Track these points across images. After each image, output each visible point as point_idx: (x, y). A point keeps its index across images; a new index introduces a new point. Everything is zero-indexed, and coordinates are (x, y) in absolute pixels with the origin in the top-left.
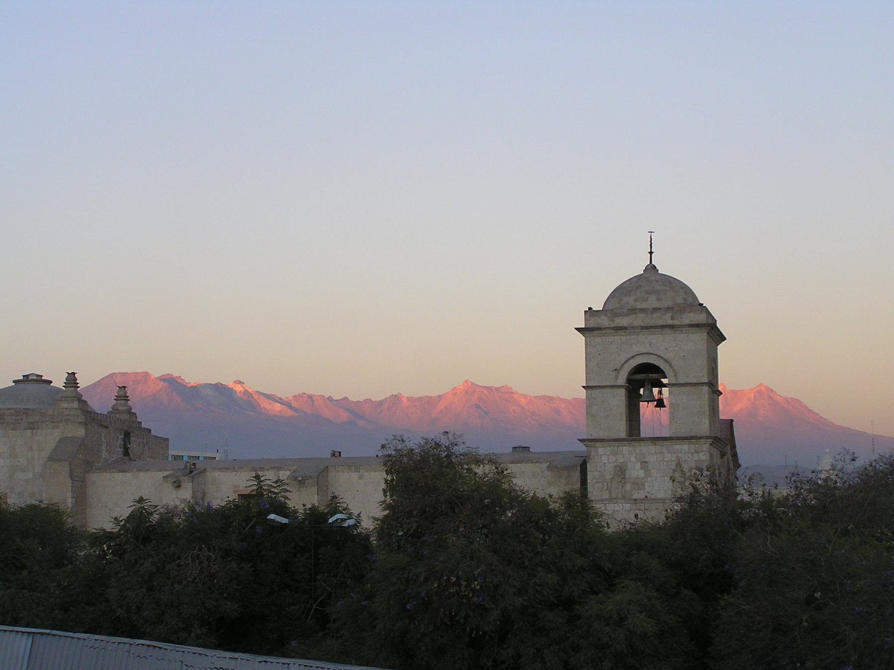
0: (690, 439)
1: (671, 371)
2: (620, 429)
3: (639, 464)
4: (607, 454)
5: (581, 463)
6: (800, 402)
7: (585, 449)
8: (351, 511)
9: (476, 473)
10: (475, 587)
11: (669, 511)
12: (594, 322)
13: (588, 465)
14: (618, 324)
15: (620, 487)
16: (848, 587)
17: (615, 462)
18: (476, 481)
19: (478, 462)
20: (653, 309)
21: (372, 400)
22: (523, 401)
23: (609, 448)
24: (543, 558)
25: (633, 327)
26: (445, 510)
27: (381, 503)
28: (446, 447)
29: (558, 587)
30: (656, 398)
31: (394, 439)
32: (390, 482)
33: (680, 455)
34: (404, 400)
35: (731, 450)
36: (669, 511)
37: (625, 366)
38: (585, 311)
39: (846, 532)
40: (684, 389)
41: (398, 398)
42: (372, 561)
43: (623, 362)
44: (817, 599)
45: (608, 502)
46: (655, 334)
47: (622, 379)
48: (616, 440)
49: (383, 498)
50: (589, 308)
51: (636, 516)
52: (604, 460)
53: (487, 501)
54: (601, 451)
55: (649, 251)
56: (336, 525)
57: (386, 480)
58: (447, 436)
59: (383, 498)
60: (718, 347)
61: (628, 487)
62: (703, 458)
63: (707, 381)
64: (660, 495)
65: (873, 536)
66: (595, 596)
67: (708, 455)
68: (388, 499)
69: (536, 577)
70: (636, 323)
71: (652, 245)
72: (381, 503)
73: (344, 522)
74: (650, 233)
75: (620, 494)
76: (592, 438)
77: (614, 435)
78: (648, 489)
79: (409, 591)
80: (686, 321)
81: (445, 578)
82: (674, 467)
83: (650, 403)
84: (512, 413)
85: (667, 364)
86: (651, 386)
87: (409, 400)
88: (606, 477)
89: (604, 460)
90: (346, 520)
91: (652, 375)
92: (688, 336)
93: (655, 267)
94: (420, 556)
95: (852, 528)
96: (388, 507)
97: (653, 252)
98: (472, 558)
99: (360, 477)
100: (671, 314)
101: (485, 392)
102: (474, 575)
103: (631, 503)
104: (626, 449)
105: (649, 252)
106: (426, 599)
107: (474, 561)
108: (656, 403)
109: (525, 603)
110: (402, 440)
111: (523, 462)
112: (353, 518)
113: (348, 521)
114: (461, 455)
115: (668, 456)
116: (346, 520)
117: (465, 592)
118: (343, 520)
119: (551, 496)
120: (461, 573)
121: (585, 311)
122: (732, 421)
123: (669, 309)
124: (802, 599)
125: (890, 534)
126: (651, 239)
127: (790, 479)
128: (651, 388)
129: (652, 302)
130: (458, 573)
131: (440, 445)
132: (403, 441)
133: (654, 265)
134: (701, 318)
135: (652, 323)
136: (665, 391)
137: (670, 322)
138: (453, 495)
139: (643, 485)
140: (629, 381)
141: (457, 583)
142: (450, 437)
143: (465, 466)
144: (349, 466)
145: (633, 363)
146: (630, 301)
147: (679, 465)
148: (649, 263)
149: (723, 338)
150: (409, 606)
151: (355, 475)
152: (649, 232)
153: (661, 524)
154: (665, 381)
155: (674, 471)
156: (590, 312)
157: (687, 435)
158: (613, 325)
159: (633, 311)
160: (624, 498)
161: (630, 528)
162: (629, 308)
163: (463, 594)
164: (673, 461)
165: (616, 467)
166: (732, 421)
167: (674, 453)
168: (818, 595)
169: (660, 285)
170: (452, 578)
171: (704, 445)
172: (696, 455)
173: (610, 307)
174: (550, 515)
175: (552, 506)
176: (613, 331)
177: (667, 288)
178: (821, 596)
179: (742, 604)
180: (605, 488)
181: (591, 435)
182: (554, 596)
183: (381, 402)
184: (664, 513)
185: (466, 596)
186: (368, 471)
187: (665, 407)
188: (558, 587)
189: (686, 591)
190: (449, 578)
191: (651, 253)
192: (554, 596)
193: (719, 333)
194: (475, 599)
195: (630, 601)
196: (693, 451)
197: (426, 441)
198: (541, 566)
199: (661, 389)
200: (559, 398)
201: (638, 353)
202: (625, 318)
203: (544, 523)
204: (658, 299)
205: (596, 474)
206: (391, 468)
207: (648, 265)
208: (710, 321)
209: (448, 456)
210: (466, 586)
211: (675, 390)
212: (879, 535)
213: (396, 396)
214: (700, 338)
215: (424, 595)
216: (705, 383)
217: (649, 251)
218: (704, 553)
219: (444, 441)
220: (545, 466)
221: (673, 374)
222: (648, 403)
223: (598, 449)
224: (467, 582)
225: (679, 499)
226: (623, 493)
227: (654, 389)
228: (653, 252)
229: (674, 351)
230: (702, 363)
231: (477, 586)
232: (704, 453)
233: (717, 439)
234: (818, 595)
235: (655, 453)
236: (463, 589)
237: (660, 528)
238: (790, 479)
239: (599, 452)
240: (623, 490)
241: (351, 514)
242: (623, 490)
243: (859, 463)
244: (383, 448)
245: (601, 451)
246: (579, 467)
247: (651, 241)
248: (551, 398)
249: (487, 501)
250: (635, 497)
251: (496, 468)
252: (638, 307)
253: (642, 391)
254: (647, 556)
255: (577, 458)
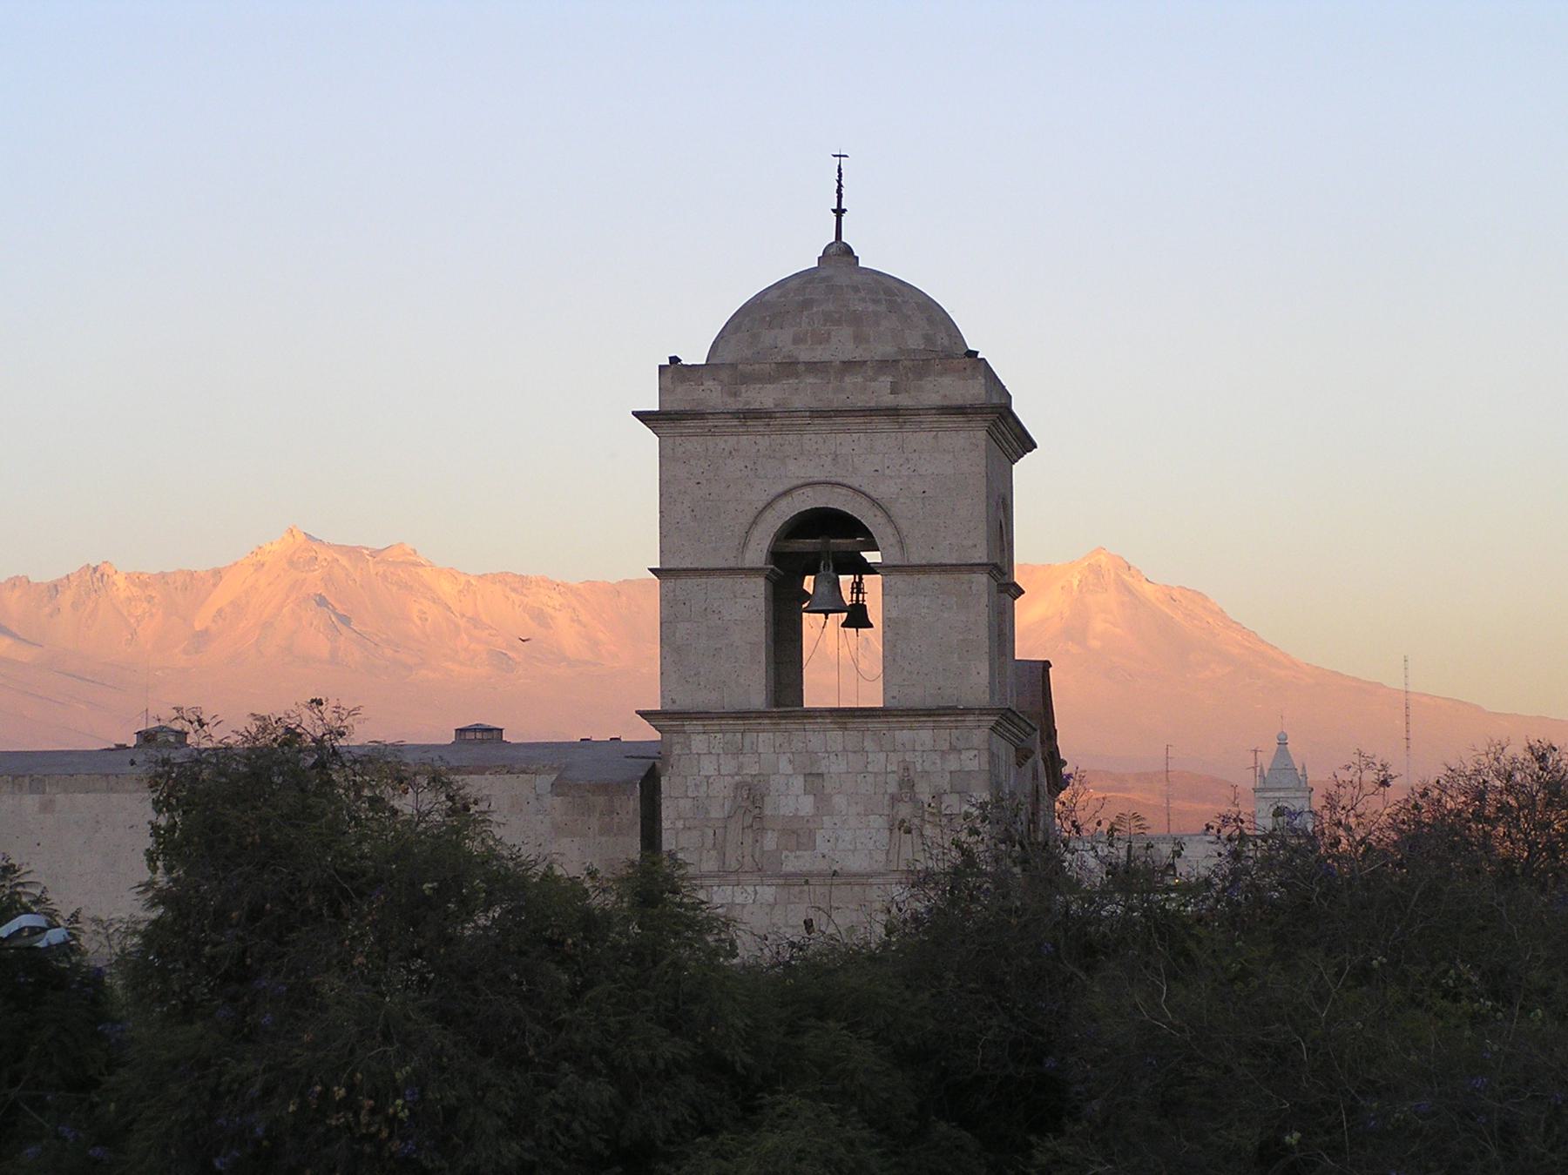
0: (939, 715)
1: (890, 530)
2: (754, 690)
3: (801, 779)
4: (713, 751)
5: (642, 774)
6: (1205, 598)
7: (657, 736)
8: (54, 907)
9: (395, 812)
10: (396, 1113)
11: (894, 910)
12: (684, 399)
13: (664, 781)
14: (748, 403)
15: (749, 840)
16: (1373, 1118)
17: (737, 774)
18: (395, 830)
19: (401, 782)
20: (844, 362)
21: (30, 579)
22: (446, 588)
23: (719, 736)
24: (578, 1038)
25: (791, 413)
26: (313, 908)
27: (142, 889)
28: (314, 740)
29: (611, 1114)
30: (848, 603)
31: (176, 718)
32: (166, 832)
33: (909, 757)
34: (121, 581)
35: (1042, 742)
36: (894, 910)
37: (769, 514)
38: (661, 367)
39: (1364, 974)
40: (925, 580)
41: (102, 575)
42: (113, 1040)
43: (761, 505)
44: (1288, 1149)
45: (717, 881)
46: (848, 431)
47: (757, 554)
48: (742, 715)
49: (146, 876)
50: (670, 358)
51: (808, 924)
52: (708, 767)
53: (430, 886)
54: (698, 743)
55: (835, 207)
56: (18, 943)
57: (155, 829)
58: (320, 711)
59: (146, 876)
60: (1014, 466)
61: (770, 841)
62: (973, 765)
63: (985, 560)
64: (856, 863)
65: (1436, 984)
66: (706, 1139)
67: (985, 757)
68: (161, 879)
69: (554, 1087)
70: (798, 402)
71: (843, 191)
72: (142, 889)
73: (39, 936)
74: (838, 158)
75: (748, 859)
76: (675, 708)
77: (734, 699)
78: (822, 846)
79: (222, 1121)
80: (934, 399)
81: (318, 1088)
82: (892, 788)
83: (830, 615)
84: (418, 622)
85: (878, 513)
86: (834, 571)
87: (133, 583)
88: (713, 814)
89: (708, 767)
90: (44, 930)
91: (839, 541)
92: (1355, 753)
93: (848, 251)
94: (246, 1030)
95: (1381, 964)
96: (161, 898)
97: (845, 211)
98: (387, 1038)
99: (46, 807)
100: (890, 379)
101: (344, 561)
102: (395, 1081)
103: (777, 885)
104: (765, 740)
105: (834, 211)
106: (265, 1143)
107: (392, 1044)
108: (845, 615)
109: (527, 1156)
110: (199, 721)
111: (488, 769)
112: (59, 926)
113: (49, 931)
114: (355, 761)
115: (877, 761)
116: (44, 930)
117: (369, 1125)
118: (36, 931)
119: (592, 874)
120: (359, 1075)
121: (661, 367)
122: (1047, 665)
123: (885, 365)
124: (1249, 1148)
125: (1475, 979)
126: (840, 176)
127: (1219, 831)
128: (833, 575)
129: (842, 346)
130: (352, 1076)
131: (300, 735)
132: (202, 724)
133: (845, 243)
134: (971, 391)
135: (838, 401)
136: (872, 583)
137: (888, 400)
138: (336, 870)
139: (811, 834)
140: (776, 556)
141: (349, 1104)
142: (328, 715)
143: (367, 792)
144: (15, 777)
145: (790, 509)
146: (781, 340)
147: (907, 783)
148: (834, 240)
149: (1027, 444)
150: (221, 1163)
151: (30, 802)
152: (835, 156)
153: (873, 946)
154: (872, 557)
155: (895, 800)
156: (673, 370)
157: (930, 703)
158: (734, 405)
159: (789, 368)
160: (760, 870)
161: (792, 957)
162: (779, 359)
163: (364, 1131)
164: (894, 772)
165: (738, 786)
166: (1047, 665)
167: (894, 751)
168: (1293, 1138)
169: (863, 300)
170: (336, 1088)
171: (975, 731)
172: (952, 757)
173: (727, 356)
174: (592, 924)
175: (596, 901)
176: (735, 422)
177: (882, 308)
178: (1299, 1142)
179: (1092, 1162)
180: (709, 842)
181: (674, 702)
182: (600, 1139)
183: (56, 586)
184: (883, 917)
185: (371, 1137)
186: (66, 791)
187: (871, 626)
188: (611, 1114)
189: (943, 1127)
190: (327, 1090)
191: (839, 212)
192: (600, 1139)
193: (1018, 430)
194: (395, 1145)
195: (799, 1151)
196: (946, 747)
197: (264, 723)
198: (566, 1060)
199: (861, 579)
200: (545, 580)
201: (799, 482)
202: (768, 386)
203: (574, 944)
204: (859, 339)
205: (685, 804)
206: (169, 796)
207: (832, 244)
208: (996, 400)
209: (321, 765)
210: (373, 1111)
211: (898, 581)
212: (1451, 983)
213: (95, 569)
214: (970, 442)
215: (261, 1133)
216: (979, 565)
217: (835, 207)
218: (991, 1026)
219: (311, 726)
220: (545, 781)
221: (893, 540)
222: (827, 618)
223: (925, 824)
224: (376, 1102)
225: (921, 880)
226: (757, 856)
227: (841, 577)
228: (845, 211)
229: (899, 477)
230: (973, 509)
231: (402, 1110)
232: (976, 752)
233: (1009, 714)
234: (1293, 1138)
235: (844, 749)
236: (364, 1118)
237: (872, 958)
238: (1219, 831)
239: (693, 747)
240: (757, 850)
241: (51, 915)
242: (757, 850)
243: (1397, 793)
244: (149, 741)
245: (698, 743)
246: (638, 786)
247: (839, 181)
248: (523, 580)
249: (430, 886)
250: (789, 867)
251: (449, 798)
252: (804, 355)
253: (809, 583)
254: (845, 1032)
255: (628, 760)
